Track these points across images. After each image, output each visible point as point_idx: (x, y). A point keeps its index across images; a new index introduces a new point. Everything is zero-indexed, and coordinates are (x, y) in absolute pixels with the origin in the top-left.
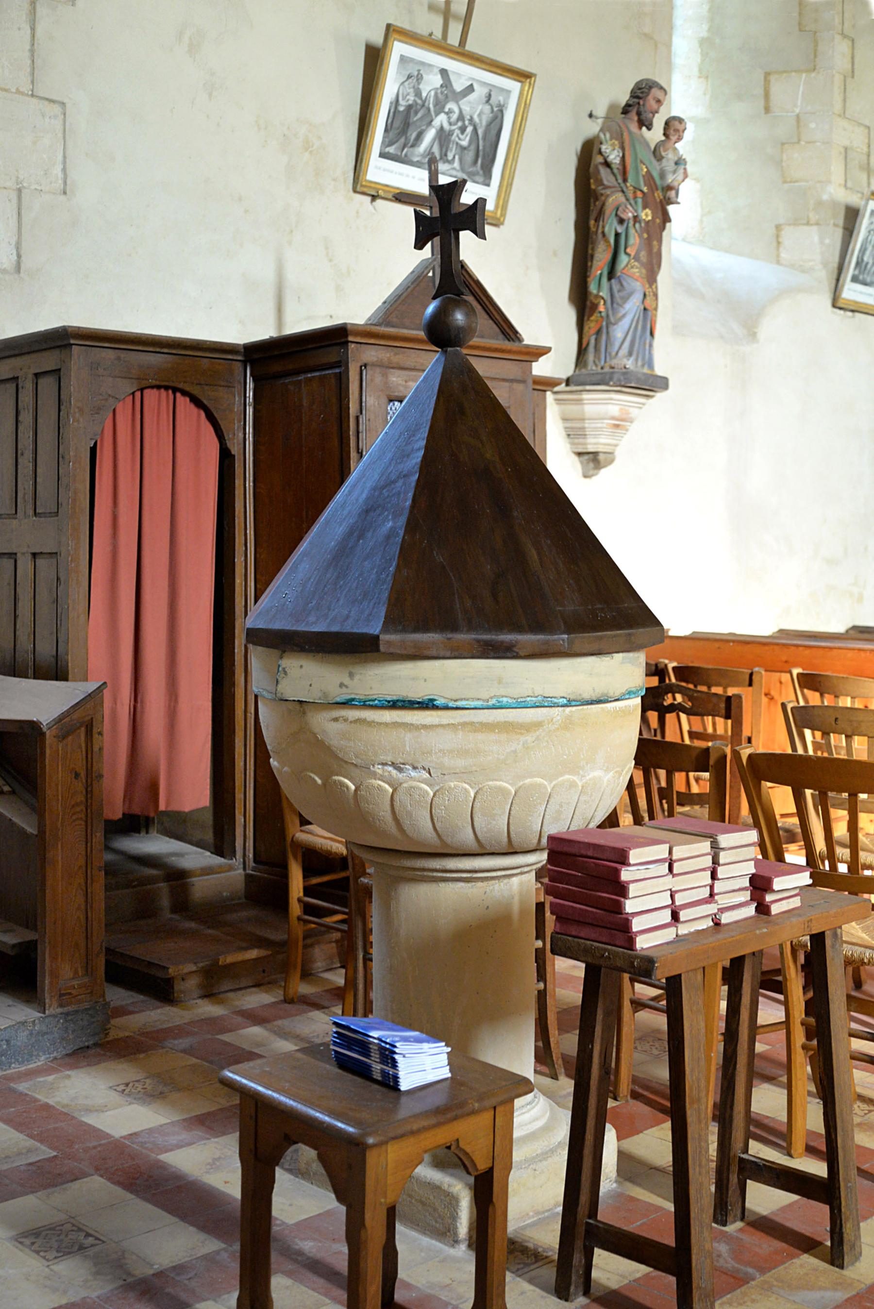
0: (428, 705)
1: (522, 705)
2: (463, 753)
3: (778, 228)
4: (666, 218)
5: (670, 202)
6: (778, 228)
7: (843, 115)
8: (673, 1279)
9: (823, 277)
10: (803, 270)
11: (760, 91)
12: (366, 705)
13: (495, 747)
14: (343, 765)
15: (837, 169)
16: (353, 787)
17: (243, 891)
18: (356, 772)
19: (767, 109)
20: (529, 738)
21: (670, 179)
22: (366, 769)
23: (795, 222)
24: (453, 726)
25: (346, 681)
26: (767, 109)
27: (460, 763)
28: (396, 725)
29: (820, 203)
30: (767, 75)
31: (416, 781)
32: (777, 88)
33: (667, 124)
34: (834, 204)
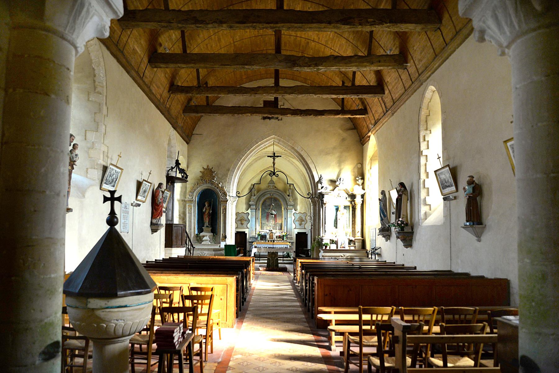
0: (126, 306)
1: (142, 304)
2: (131, 315)
3: (87, 169)
4: (73, 169)
5: (74, 164)
6: (87, 169)
7: (103, 143)
8: (477, 198)
9: (98, 182)
10: (94, 180)
11: (84, 134)
12: (112, 308)
13: (137, 313)
14: (103, 321)
15: (102, 156)
16: (105, 326)
17: (245, 320)
18: (107, 323)
19: (85, 139)
20: (142, 311)
21: (75, 159)
22: (110, 322)
23: (91, 168)
24: (129, 310)
25: (107, 303)
26: (85, 139)
27: (131, 318)
28: (118, 311)
29: (97, 164)
30: (86, 131)
31: (121, 323)
32: (89, 134)
33: (74, 145)
34: (101, 164)
